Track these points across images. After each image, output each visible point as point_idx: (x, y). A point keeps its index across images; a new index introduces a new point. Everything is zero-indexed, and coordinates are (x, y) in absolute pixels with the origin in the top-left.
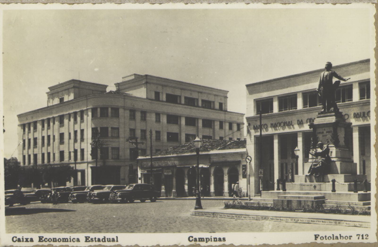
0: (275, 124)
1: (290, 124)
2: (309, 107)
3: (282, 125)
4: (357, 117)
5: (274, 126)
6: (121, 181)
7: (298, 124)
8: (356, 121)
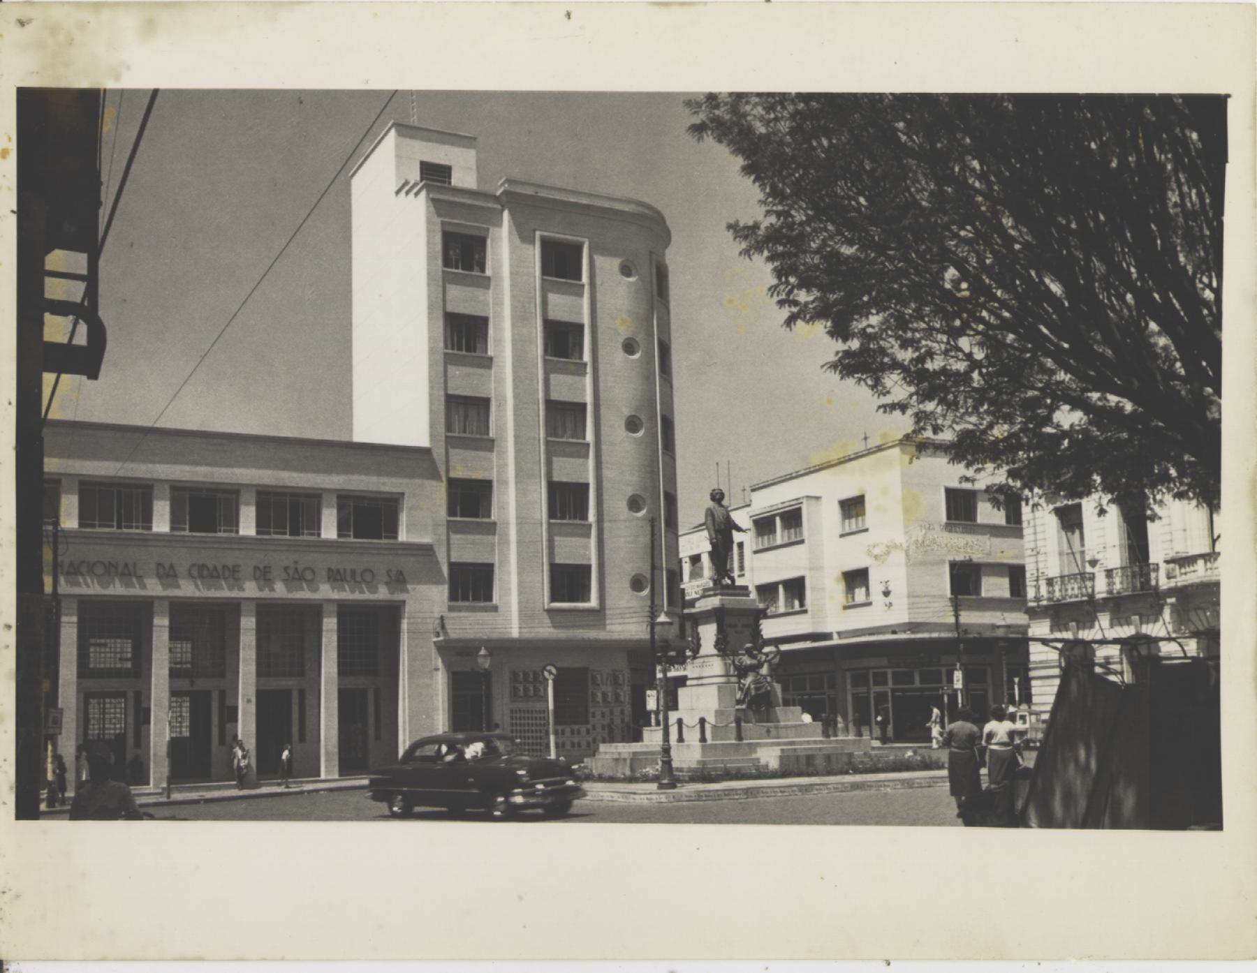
0: (71, 564)
1: (128, 573)
2: (355, 537)
3: (99, 570)
4: (335, 580)
5: (336, 577)
6: (560, 728)
7: (159, 577)
8: (333, 589)
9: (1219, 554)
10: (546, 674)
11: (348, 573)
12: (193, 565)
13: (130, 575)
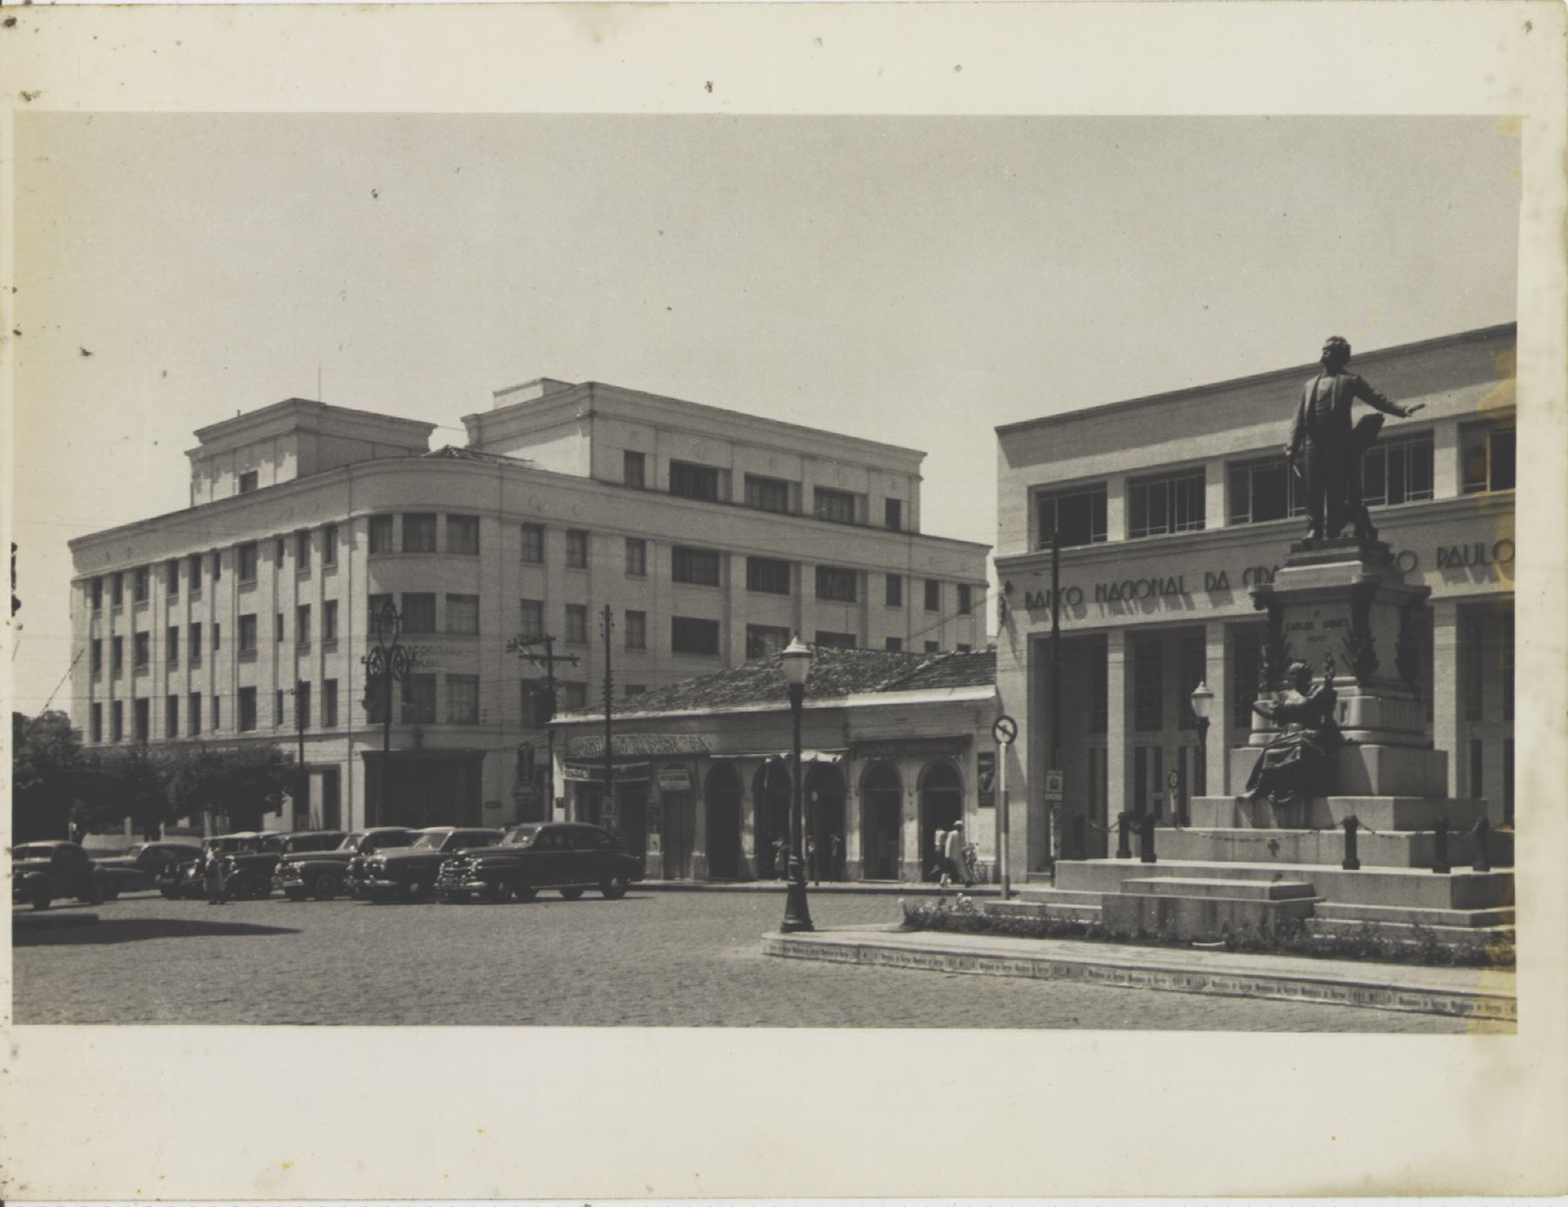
0: (1114, 586)
1: (1173, 590)
3: (1143, 590)
4: (1449, 566)
9: (200, 433)
10: (999, 733)
11: (1472, 551)
12: (1248, 570)
13: (1175, 593)
